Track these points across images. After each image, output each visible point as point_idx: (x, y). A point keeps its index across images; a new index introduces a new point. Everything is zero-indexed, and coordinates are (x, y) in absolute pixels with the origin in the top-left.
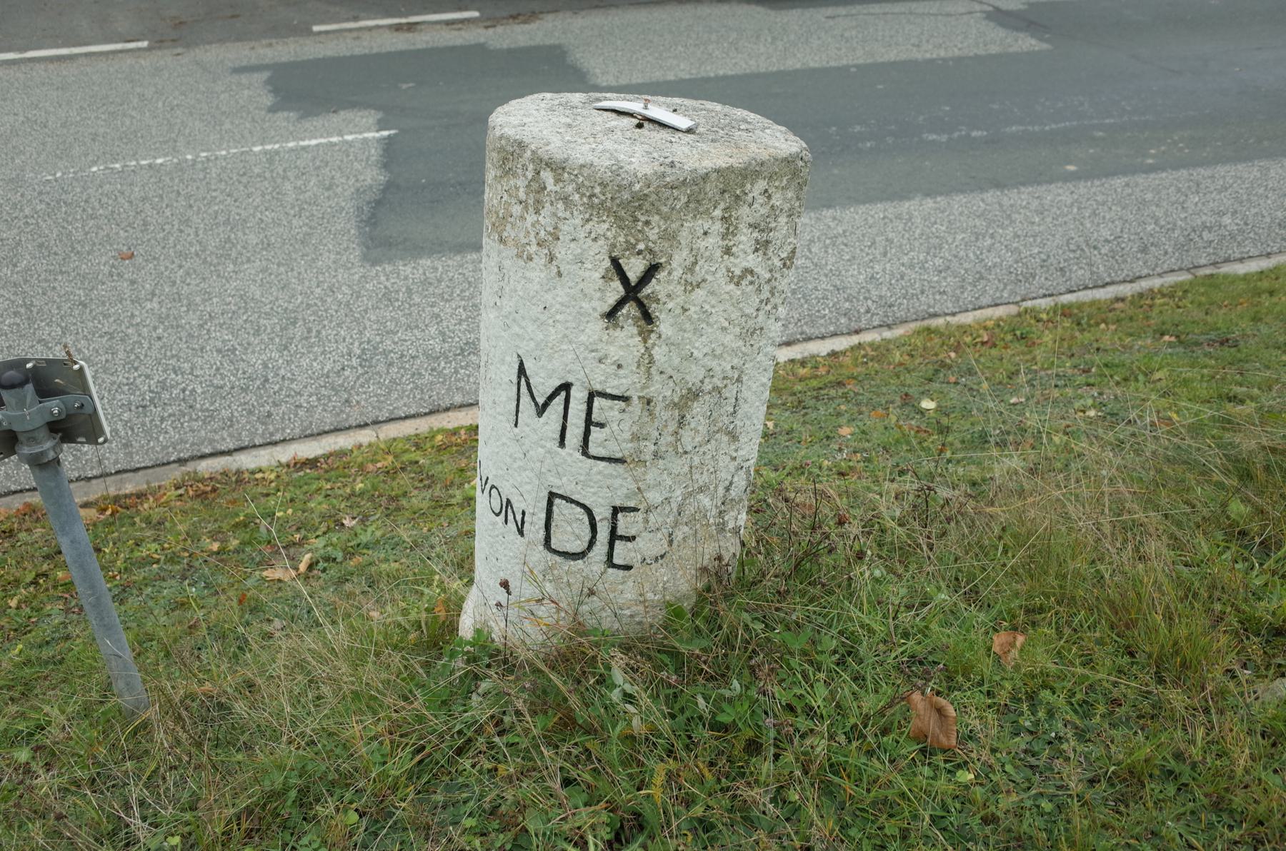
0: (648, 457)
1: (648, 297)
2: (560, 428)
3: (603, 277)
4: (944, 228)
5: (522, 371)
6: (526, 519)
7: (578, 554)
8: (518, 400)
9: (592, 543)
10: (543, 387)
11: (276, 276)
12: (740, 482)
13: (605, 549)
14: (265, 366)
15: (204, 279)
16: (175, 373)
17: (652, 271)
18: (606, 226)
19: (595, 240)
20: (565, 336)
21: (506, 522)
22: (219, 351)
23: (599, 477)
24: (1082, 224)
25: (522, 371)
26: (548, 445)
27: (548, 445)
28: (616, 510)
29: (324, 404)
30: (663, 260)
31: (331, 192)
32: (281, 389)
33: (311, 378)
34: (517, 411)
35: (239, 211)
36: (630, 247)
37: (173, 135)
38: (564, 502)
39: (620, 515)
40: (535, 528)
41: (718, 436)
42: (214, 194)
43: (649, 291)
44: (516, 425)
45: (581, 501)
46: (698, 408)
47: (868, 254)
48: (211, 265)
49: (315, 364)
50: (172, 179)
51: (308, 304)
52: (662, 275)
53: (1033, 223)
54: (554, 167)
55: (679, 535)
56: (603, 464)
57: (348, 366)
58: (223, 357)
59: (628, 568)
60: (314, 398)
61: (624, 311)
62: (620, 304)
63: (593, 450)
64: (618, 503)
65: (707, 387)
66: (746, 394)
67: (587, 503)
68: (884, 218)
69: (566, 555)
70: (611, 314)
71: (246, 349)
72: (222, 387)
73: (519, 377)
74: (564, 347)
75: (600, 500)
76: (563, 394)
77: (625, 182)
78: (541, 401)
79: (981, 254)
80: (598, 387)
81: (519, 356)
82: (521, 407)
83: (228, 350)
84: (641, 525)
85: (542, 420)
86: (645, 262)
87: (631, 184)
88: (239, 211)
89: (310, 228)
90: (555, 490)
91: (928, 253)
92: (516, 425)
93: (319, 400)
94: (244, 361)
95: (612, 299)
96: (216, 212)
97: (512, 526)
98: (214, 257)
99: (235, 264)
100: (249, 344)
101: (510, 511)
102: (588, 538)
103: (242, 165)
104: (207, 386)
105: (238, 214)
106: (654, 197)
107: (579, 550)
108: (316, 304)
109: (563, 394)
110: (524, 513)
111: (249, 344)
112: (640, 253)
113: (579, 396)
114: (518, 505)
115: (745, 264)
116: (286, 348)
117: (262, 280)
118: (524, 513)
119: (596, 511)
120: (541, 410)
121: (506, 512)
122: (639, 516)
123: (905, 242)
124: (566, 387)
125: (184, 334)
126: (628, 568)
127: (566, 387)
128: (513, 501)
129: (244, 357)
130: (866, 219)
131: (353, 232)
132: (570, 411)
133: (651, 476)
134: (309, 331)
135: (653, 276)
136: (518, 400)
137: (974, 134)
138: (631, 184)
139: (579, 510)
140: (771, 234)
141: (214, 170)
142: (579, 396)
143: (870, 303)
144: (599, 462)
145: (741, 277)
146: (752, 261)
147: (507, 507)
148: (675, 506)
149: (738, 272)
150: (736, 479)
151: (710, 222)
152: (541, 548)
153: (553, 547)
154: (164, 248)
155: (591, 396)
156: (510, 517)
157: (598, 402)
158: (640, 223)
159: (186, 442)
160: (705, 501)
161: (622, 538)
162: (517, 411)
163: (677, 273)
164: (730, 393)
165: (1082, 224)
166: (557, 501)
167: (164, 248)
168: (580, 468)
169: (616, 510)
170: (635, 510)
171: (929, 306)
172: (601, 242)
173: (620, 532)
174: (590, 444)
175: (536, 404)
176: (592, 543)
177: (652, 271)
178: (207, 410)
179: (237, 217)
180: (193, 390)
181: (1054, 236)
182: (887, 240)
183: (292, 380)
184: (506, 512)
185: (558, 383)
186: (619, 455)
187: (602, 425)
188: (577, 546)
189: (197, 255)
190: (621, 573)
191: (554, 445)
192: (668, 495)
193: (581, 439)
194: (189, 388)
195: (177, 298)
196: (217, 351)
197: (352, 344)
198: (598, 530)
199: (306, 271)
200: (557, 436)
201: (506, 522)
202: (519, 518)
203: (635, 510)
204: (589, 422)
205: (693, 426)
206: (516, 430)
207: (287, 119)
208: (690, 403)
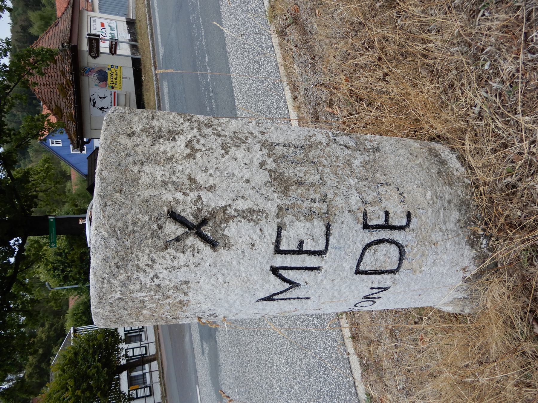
0: (324, 207)
1: (196, 216)
2: (307, 271)
3: (183, 252)
4: (242, 66)
5: (269, 299)
6: (376, 287)
7: (400, 250)
8: (290, 299)
9: (391, 242)
10: (278, 285)
11: (278, 348)
12: (343, 140)
13: (396, 232)
14: (314, 358)
15: (280, 380)
16: (320, 398)
17: (174, 216)
18: (140, 254)
19: (153, 260)
20: (235, 274)
21: (379, 298)
22: (310, 377)
23: (342, 241)
24: (237, 7)
25: (269, 299)
26: (320, 278)
27: (320, 278)
28: (366, 226)
29: (330, 334)
30: (166, 209)
31: (244, 322)
32: (324, 352)
33: (319, 338)
34: (298, 298)
35: (253, 361)
36: (154, 234)
37: (227, 383)
38: (362, 264)
39: (370, 223)
40: (385, 280)
41: (311, 158)
42: (247, 370)
43: (191, 218)
44: (308, 298)
45: (361, 252)
46: (289, 172)
47: (254, 98)
48: (274, 376)
49: (313, 336)
50: (243, 386)
51: (288, 336)
52: (178, 210)
53: (238, 28)
54: (101, 294)
55: (383, 179)
56: (331, 239)
57: (313, 322)
58: (312, 376)
59: (409, 215)
60: (327, 338)
61: (209, 234)
62: (204, 238)
63: (322, 247)
64: (360, 226)
65: (273, 166)
66: (281, 140)
67: (361, 248)
68: (240, 93)
69: (401, 260)
70: (213, 244)
71: (308, 366)
72: (325, 379)
73: (274, 300)
74: (244, 275)
75: (359, 239)
76: (281, 272)
77: (103, 243)
78: (288, 286)
79: (251, 48)
80: (272, 247)
81: (257, 301)
82: (294, 297)
83: (309, 374)
84: (376, 208)
85: (302, 283)
86: (167, 223)
87: (103, 238)
88: (253, 361)
89: (258, 332)
90: (354, 270)
91: (252, 72)
92: (308, 298)
93: (328, 336)
94: (313, 367)
95: (200, 244)
96: (254, 370)
97: (381, 294)
98: (271, 374)
99: (274, 365)
100: (306, 364)
101: (371, 296)
102: (387, 245)
103: (236, 357)
104: (325, 385)
105: (254, 362)
106: (112, 220)
107: (397, 250)
108: (288, 333)
109: (281, 272)
110: (372, 288)
111: (306, 364)
112: (160, 227)
113: (280, 261)
114: (368, 292)
115: (184, 145)
116: (306, 348)
117: (279, 355)
118: (372, 288)
119: (367, 241)
120: (293, 285)
121: (371, 298)
122: (370, 209)
123: (249, 83)
124: (275, 270)
125: (303, 391)
126: (409, 215)
127: (275, 270)
128: (364, 295)
129: (311, 367)
130: (241, 100)
131: (223, 361)
132: (293, 265)
133: (339, 202)
134: (298, 337)
135: (179, 215)
136: (290, 299)
137: (207, 60)
138: (103, 238)
139: (367, 253)
140: (164, 130)
141: (238, 369)
142: (280, 261)
143: (273, 94)
144: (330, 242)
145: (192, 148)
146: (181, 142)
147: (369, 298)
148: (362, 184)
149: (188, 151)
150: (342, 142)
151: (143, 174)
152: (397, 276)
153: (394, 247)
154: (269, 394)
155: (278, 251)
156: (376, 296)
157: (284, 247)
158: (135, 228)
159: (351, 399)
160: (356, 163)
161: (387, 220)
162: (298, 298)
163: (179, 196)
164: (280, 150)
165: (237, 7)
166: (362, 268)
167: (269, 394)
168: (335, 255)
169: (366, 226)
170: (365, 214)
171: (274, 67)
172: (155, 256)
173: (381, 222)
174: (285, 289)
175: (291, 288)
176: (391, 242)
177: (174, 216)
178: (336, 387)
179: (255, 362)
180: (327, 391)
181: (242, 18)
182: (248, 90)
183: (320, 347)
184: (371, 298)
185: (272, 276)
186: (324, 229)
187: (301, 243)
188: (394, 251)
189: (271, 381)
190: (413, 220)
191: (319, 276)
192: (353, 189)
193: (313, 256)
194: (326, 393)
195: (289, 392)
196: (309, 378)
197: (303, 319)
198: (381, 238)
199: (274, 336)
200: (312, 273)
201: (379, 298)
202: (375, 291)
203: (365, 214)
204: (300, 252)
205: (301, 175)
206: (312, 298)
207: (219, 337)
208: (285, 179)
